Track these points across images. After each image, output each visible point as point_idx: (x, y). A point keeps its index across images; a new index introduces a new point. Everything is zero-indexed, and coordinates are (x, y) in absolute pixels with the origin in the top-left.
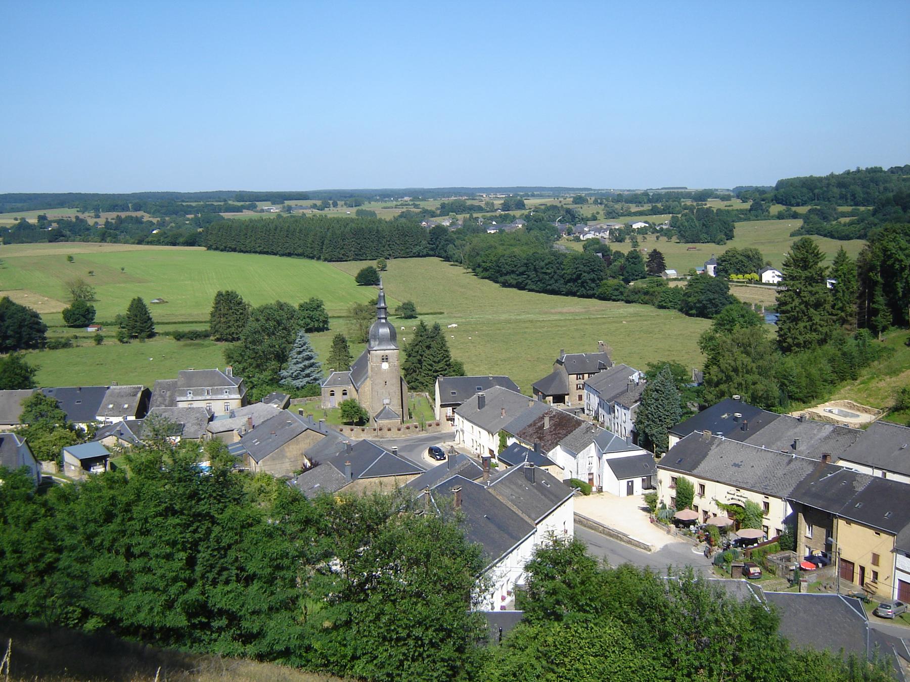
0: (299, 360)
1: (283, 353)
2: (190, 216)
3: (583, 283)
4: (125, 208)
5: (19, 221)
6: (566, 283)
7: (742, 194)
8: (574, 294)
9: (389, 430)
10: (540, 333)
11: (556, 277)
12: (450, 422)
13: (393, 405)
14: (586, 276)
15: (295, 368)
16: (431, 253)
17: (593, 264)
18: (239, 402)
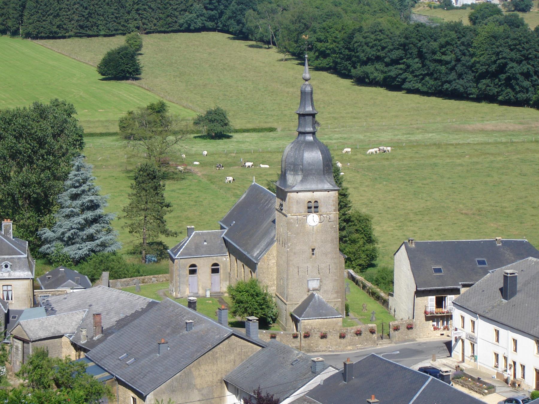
0: (77, 210)
1: (46, 196)
3: (508, 79)
6: (477, 80)
8: (491, 99)
9: (324, 336)
10: (461, 165)
11: (459, 68)
12: (431, 322)
13: (326, 292)
14: (514, 68)
15: (67, 223)
16: (210, 24)
17: (527, 46)
18: (28, 283)
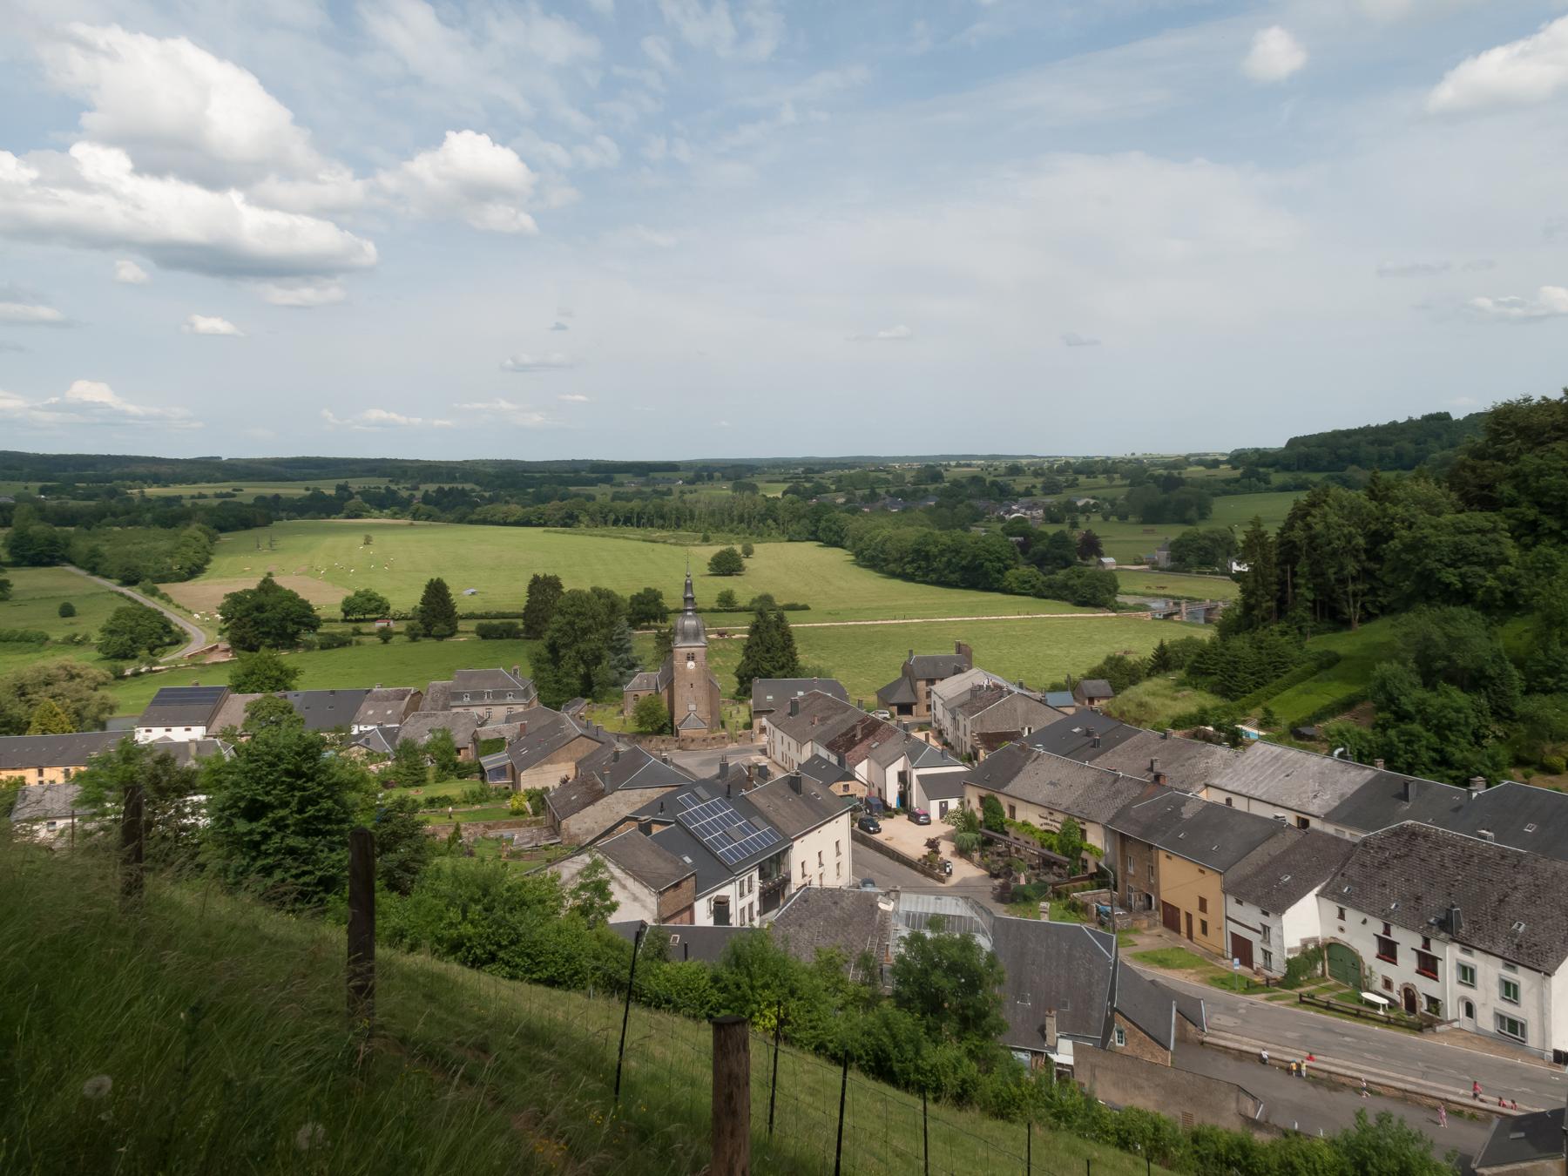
2: (531, 490)
4: (453, 479)
5: (310, 492)
7: (1237, 458)
